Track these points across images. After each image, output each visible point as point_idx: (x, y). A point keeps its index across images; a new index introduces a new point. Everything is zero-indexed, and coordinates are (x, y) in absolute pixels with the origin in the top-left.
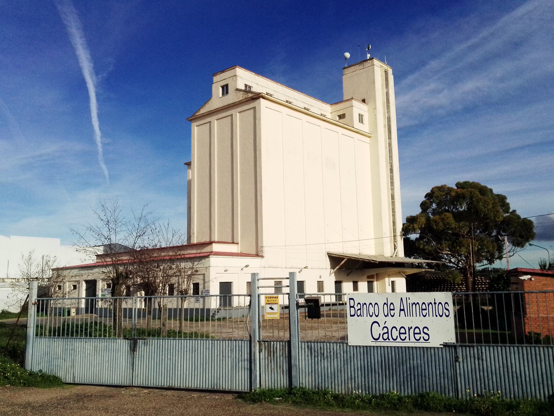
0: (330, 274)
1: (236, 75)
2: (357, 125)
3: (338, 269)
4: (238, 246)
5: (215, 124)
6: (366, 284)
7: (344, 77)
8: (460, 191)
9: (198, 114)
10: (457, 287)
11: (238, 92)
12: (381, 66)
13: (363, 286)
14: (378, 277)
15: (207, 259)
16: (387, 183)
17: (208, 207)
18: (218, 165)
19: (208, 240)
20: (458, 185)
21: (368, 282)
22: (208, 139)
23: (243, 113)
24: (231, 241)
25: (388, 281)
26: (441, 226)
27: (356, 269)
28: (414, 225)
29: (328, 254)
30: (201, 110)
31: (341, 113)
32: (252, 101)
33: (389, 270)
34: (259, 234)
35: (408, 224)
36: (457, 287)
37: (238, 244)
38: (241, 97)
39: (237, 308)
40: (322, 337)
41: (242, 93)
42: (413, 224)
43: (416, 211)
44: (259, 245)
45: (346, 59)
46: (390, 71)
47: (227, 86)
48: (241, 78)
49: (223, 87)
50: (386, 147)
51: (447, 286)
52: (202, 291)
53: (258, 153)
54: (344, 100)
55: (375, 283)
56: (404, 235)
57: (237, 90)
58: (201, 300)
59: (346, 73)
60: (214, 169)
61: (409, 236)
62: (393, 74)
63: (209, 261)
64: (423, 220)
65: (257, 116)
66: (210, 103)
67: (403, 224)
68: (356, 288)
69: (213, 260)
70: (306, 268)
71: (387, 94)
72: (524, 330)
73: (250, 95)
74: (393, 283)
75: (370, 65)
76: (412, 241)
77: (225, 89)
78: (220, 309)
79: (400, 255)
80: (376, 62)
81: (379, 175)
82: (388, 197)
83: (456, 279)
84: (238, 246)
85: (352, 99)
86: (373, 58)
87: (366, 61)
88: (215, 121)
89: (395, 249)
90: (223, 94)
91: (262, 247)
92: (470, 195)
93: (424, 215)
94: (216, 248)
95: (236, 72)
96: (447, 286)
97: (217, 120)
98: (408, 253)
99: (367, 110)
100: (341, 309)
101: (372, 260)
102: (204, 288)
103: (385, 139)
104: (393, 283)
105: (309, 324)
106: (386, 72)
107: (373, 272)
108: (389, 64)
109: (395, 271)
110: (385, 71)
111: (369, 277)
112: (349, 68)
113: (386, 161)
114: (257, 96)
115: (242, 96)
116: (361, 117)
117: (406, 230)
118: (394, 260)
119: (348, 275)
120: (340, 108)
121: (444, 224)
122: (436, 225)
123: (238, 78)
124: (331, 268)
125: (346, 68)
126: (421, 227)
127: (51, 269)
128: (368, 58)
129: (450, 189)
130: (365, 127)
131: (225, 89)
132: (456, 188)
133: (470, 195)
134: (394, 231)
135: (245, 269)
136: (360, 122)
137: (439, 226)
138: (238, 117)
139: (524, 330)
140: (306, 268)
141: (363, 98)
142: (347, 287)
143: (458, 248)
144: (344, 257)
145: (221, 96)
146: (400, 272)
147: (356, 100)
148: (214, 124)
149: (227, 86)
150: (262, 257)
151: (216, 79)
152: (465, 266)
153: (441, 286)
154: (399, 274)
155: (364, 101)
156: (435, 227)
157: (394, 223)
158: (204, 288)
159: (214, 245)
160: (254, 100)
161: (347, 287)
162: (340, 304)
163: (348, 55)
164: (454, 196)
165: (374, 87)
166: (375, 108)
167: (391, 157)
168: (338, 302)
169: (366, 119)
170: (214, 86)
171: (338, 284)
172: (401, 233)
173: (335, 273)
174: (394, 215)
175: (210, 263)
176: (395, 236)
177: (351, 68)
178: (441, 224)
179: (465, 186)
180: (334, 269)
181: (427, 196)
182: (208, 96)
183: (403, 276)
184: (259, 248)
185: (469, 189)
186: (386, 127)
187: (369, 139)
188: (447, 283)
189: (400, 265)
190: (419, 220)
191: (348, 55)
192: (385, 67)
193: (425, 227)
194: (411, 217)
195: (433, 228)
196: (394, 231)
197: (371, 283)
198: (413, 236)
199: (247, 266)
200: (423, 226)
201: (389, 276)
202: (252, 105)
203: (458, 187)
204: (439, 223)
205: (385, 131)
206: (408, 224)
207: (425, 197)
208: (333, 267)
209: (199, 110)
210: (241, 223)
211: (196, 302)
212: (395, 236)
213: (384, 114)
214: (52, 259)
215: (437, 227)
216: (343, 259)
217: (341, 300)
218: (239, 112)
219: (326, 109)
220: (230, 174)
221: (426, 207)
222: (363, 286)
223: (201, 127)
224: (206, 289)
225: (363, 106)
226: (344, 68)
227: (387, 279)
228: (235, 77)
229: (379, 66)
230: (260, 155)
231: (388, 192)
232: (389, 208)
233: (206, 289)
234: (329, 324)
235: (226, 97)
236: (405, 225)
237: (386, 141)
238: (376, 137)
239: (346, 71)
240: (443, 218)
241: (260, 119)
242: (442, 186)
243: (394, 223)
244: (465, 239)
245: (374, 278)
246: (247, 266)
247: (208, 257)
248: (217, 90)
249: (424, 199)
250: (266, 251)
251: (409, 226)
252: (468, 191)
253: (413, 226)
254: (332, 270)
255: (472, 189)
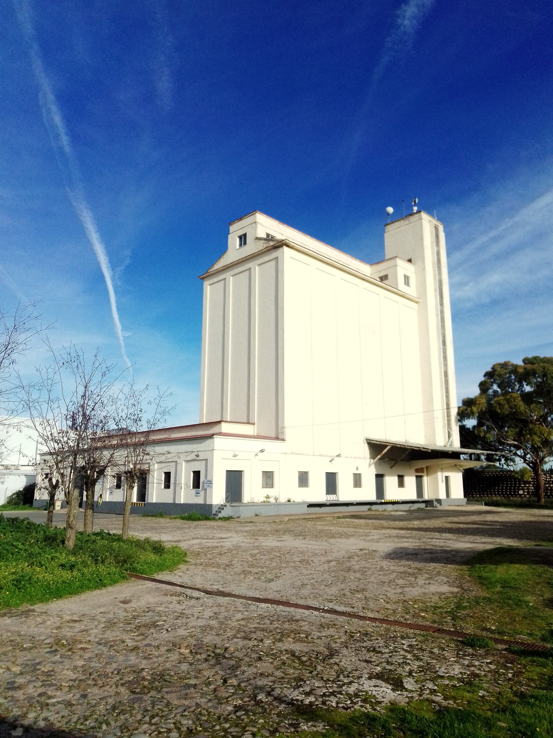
0: (370, 465)
1: (255, 222)
2: (402, 286)
3: (380, 459)
4: (254, 427)
5: (231, 281)
6: (413, 479)
7: (386, 235)
8: (529, 366)
9: (211, 270)
10: (523, 485)
11: (257, 241)
12: (430, 221)
13: (410, 481)
14: (428, 470)
15: (209, 441)
16: (439, 358)
17: (220, 381)
18: (233, 329)
19: (220, 420)
20: (526, 361)
21: (417, 477)
22: (222, 299)
23: (263, 266)
24: (246, 422)
25: (441, 476)
26: (507, 409)
27: (402, 460)
28: (473, 408)
29: (367, 440)
30: (215, 266)
31: (382, 274)
32: (274, 250)
33: (439, 463)
34: (280, 412)
35: (465, 407)
36: (523, 485)
37: (254, 424)
38: (261, 246)
39: (252, 504)
40: (357, 551)
41: (262, 242)
42: (471, 408)
43: (474, 392)
44: (280, 426)
45: (388, 214)
46: (441, 228)
47: (245, 235)
48: (262, 225)
49: (240, 237)
50: (437, 315)
51: (511, 484)
52: (203, 482)
53: (280, 312)
54: (386, 258)
55: (425, 479)
56: (459, 421)
57: (258, 239)
58: (202, 493)
59: (389, 230)
60: (228, 334)
61: (464, 423)
62: (444, 231)
63: (214, 442)
64: (484, 401)
65: (280, 268)
66: (225, 256)
67: (459, 408)
68: (401, 484)
69: (218, 441)
70: (338, 456)
71: (438, 253)
72: (476, 526)
73: (272, 243)
74: (447, 478)
75: (417, 219)
76: (468, 429)
77: (243, 239)
78: (225, 506)
79: (456, 444)
80: (424, 216)
81: (428, 347)
82: (441, 374)
83: (526, 476)
84: (254, 427)
85: (396, 257)
86: (421, 211)
87: (412, 214)
88: (230, 278)
89: (449, 437)
90: (241, 245)
91: (283, 428)
92: (543, 372)
93: (484, 396)
94: (225, 428)
95: (255, 218)
96: (511, 484)
97: (232, 276)
98: (464, 444)
99: (413, 271)
100: (383, 509)
101: (423, 448)
102: (206, 478)
103: (436, 305)
104: (447, 478)
105: (339, 529)
106: (436, 228)
107: (422, 464)
108: (440, 219)
109: (450, 464)
110: (436, 227)
111: (417, 471)
112: (392, 225)
113: (438, 331)
114: (280, 244)
115: (262, 245)
116: (407, 280)
117: (462, 415)
118: (448, 449)
119: (392, 467)
120: (381, 269)
121: (510, 407)
122: (500, 408)
123: (259, 226)
124: (371, 458)
125: (388, 224)
126: (481, 410)
127: (40, 454)
128: (415, 211)
129: (516, 367)
130: (411, 291)
131: (243, 239)
132: (522, 364)
133: (543, 372)
134: (449, 416)
135: (260, 454)
136: (405, 284)
137: (504, 409)
138: (257, 271)
139: (476, 526)
140: (338, 456)
141: (409, 257)
142: (391, 481)
143: (528, 436)
144: (387, 444)
145: (238, 247)
146: (456, 465)
147: (400, 258)
148: (230, 280)
149: (245, 235)
150: (283, 440)
151: (232, 228)
152: (536, 460)
153: (503, 484)
154: (455, 468)
155: (410, 261)
156: (499, 411)
157: (448, 408)
158: (206, 478)
159: (223, 424)
160: (276, 250)
161: (391, 481)
162: (382, 503)
163: (390, 210)
164: (522, 373)
165: (423, 244)
166: (424, 269)
167: (443, 327)
168: (379, 501)
169: (412, 281)
170: (230, 236)
171: (379, 477)
172: (456, 418)
173: (376, 464)
174: (447, 397)
175: (214, 445)
176: (449, 421)
177: (394, 224)
178: (506, 406)
179: (535, 361)
180: (374, 459)
181: (488, 374)
182: (223, 248)
183: (460, 470)
184: (280, 429)
185: (542, 364)
186: (436, 291)
187: (416, 305)
188: (515, 482)
189: (455, 455)
190: (478, 402)
191: (390, 210)
192: (435, 222)
193: (485, 411)
194: (469, 399)
195: (497, 412)
196: (449, 416)
197: (419, 479)
198: (470, 423)
199: (262, 451)
200: (484, 409)
201: (442, 470)
202: (274, 255)
203: (525, 363)
204: (504, 405)
205: (436, 296)
206: (465, 407)
207: (485, 376)
208: (373, 457)
209: (213, 266)
210: (259, 398)
211: (196, 496)
212: (449, 421)
213: (435, 276)
214: (54, 446)
215: (501, 410)
216: (387, 446)
217: (383, 499)
218: (259, 265)
219: (365, 269)
220: (247, 339)
221: (486, 387)
222: (410, 481)
223: (214, 285)
224: (208, 479)
225: (408, 265)
226: (386, 225)
227: (439, 474)
228: (254, 225)
229: (428, 220)
230: (283, 314)
231: (440, 368)
232: (442, 387)
233: (208, 479)
234: (367, 529)
235: (245, 248)
236: (461, 409)
237: (437, 308)
238: (425, 302)
239: (389, 228)
240: (509, 399)
241: (283, 271)
242: (505, 363)
243: (448, 408)
244: (537, 426)
245: (423, 472)
246: (262, 451)
247: (211, 436)
248: (233, 241)
249: (483, 379)
250: (288, 434)
251: (466, 410)
252: (539, 366)
253: (472, 410)
254: (372, 460)
255: (546, 365)
